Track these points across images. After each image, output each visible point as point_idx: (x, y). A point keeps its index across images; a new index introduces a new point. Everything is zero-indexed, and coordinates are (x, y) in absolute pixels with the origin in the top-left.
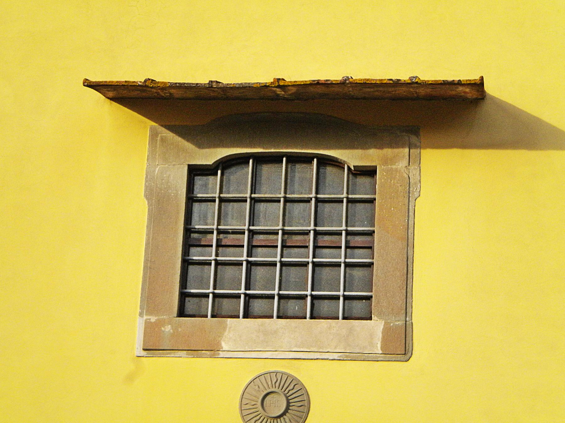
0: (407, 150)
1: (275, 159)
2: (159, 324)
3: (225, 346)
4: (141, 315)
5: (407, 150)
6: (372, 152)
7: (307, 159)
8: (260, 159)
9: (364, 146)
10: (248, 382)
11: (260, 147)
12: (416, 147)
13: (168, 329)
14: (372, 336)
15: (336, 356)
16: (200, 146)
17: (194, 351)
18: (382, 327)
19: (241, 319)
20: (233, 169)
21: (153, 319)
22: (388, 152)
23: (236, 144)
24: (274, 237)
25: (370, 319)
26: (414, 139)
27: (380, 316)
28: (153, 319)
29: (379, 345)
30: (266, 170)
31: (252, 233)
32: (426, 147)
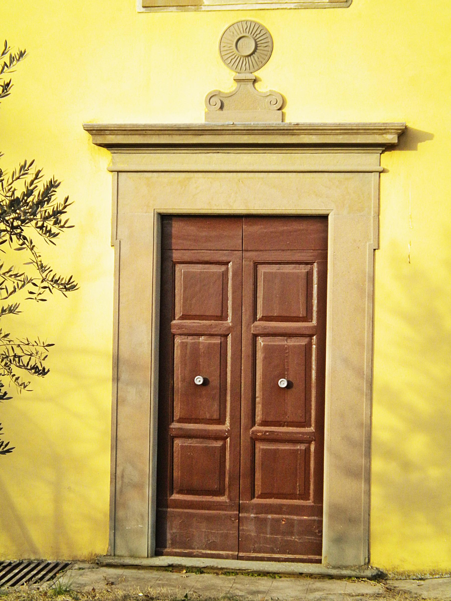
15: (292, 6)
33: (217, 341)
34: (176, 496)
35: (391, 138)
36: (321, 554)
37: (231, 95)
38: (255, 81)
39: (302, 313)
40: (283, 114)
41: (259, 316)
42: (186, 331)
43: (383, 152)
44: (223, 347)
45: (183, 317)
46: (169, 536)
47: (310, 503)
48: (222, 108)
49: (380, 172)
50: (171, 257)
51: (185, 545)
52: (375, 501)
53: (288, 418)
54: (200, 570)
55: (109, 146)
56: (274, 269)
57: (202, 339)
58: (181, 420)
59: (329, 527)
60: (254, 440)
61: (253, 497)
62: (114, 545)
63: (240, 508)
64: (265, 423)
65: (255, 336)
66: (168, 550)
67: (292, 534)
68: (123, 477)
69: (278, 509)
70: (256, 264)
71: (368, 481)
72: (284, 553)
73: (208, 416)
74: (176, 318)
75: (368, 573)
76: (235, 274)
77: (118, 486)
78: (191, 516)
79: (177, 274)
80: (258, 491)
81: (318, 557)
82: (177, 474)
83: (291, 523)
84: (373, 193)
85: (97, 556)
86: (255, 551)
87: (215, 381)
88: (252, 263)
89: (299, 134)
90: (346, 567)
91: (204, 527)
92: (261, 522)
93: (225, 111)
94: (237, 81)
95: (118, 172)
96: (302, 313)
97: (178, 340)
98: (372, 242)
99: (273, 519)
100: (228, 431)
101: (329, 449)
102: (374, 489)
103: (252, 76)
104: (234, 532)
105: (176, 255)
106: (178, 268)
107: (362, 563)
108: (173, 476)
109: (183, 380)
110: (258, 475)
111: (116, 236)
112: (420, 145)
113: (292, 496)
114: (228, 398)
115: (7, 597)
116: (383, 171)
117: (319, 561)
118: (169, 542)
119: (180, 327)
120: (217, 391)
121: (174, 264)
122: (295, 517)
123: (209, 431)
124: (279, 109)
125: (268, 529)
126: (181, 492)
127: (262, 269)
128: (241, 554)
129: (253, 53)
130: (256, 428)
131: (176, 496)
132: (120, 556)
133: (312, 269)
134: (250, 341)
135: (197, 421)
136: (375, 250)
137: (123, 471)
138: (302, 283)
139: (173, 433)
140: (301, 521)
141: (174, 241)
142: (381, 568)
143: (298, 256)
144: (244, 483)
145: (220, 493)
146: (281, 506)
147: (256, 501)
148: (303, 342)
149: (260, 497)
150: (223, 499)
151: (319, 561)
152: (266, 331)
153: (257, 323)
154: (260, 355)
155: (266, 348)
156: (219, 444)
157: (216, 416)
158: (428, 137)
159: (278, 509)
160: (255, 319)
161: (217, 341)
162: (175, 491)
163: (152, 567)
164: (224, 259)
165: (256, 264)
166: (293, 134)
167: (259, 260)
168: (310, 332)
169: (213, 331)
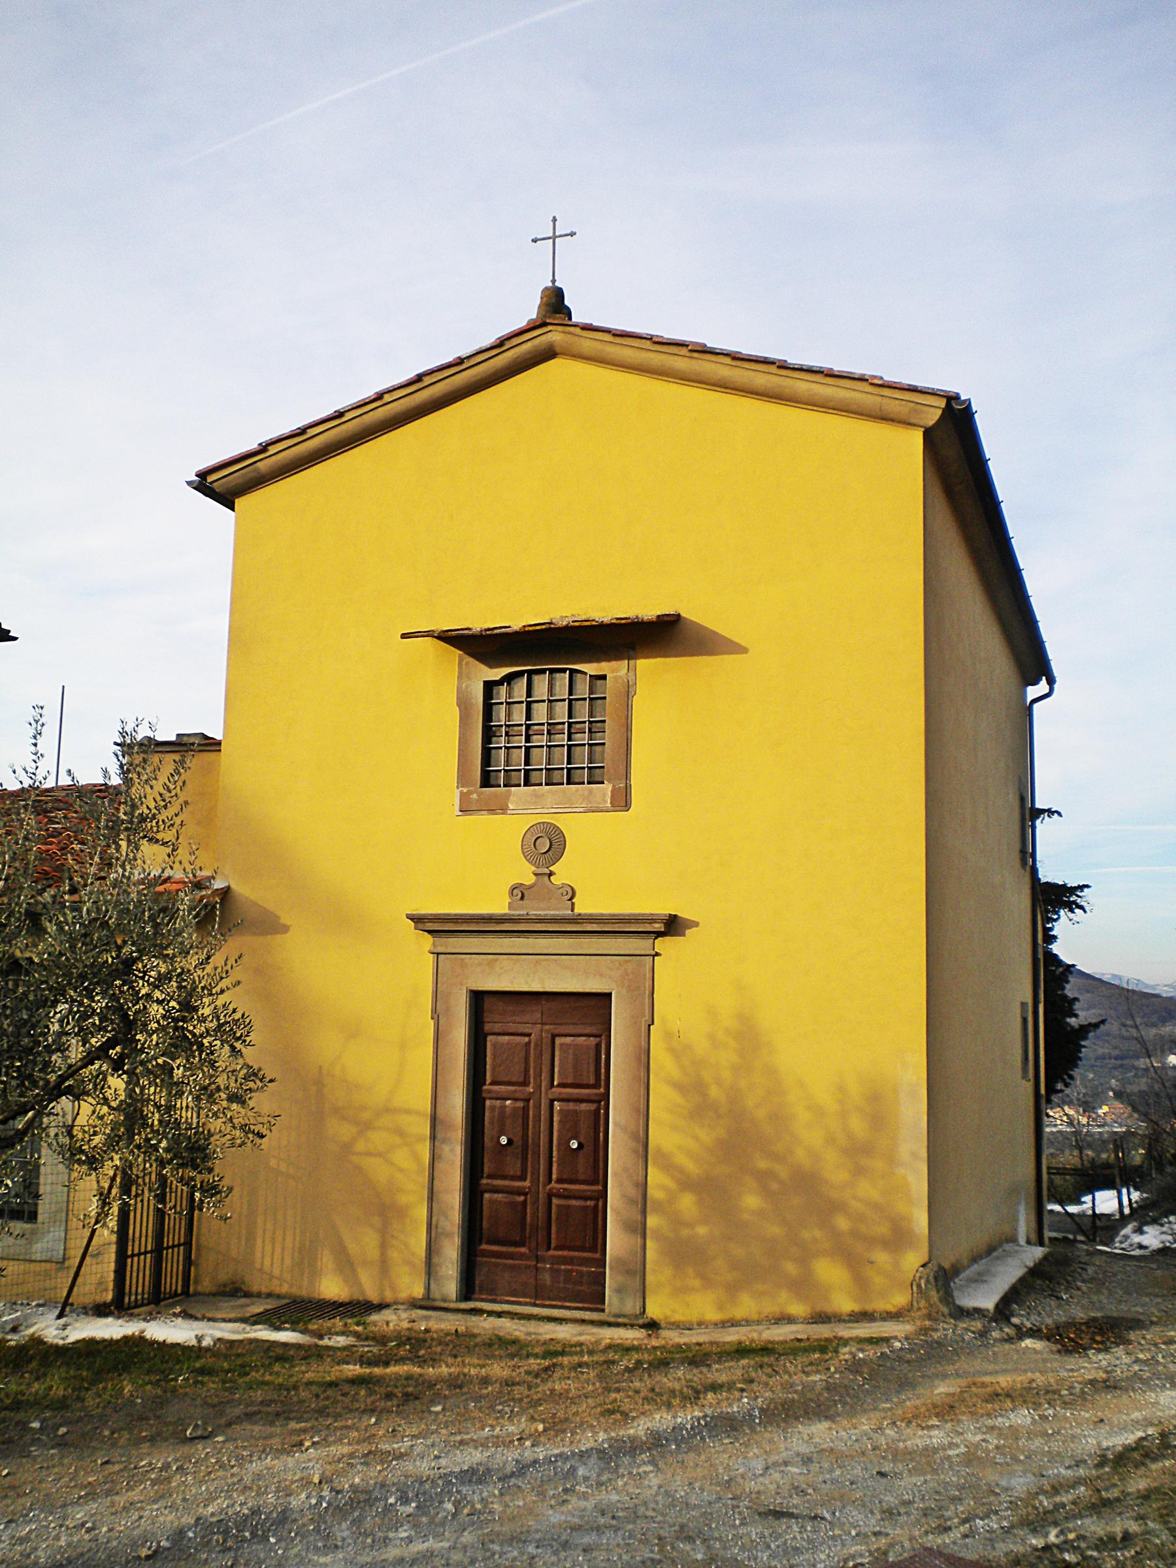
0: (626, 662)
1: (543, 671)
2: (469, 793)
3: (511, 807)
4: (458, 787)
5: (626, 662)
6: (604, 664)
7: (563, 671)
8: (531, 673)
9: (598, 661)
10: (639, 915)
11: (529, 665)
12: (633, 659)
13: (475, 796)
14: (604, 795)
15: (581, 810)
16: (491, 667)
17: (492, 811)
18: (610, 789)
19: (522, 788)
20: (516, 680)
21: (465, 790)
22: (614, 664)
23: (40, 942)
24: (583, 725)
25: (603, 783)
26: (631, 653)
27: (609, 782)
28: (465, 790)
29: (609, 801)
30: (536, 678)
31: (570, 724)
32: (639, 659)
33: (520, 1104)
34: (484, 1247)
35: (659, 927)
36: (604, 1303)
37: (531, 887)
38: (551, 874)
39: (592, 1081)
40: (573, 904)
41: (556, 1083)
42: (494, 1096)
43: (656, 938)
44: (525, 1110)
45: (493, 1083)
46: (477, 1282)
47: (598, 1256)
48: (522, 898)
49: (654, 956)
50: (483, 1029)
51: (492, 1291)
52: (650, 1254)
53: (581, 1177)
54: (499, 1315)
55: (429, 932)
56: (569, 1040)
57: (508, 1102)
58: (490, 1177)
59: (610, 1277)
60: (550, 1196)
61: (549, 1249)
62: (428, 1288)
63: (538, 1259)
64: (559, 1181)
65: (552, 1101)
66: (476, 1296)
67: (581, 1284)
68: (437, 1227)
69: (569, 1261)
70: (554, 1037)
71: (644, 1237)
72: (575, 1301)
73: (512, 1173)
74: (488, 1082)
75: (641, 1321)
76: (536, 1045)
77: (433, 1235)
78: (496, 1265)
79: (489, 1044)
80: (553, 1244)
81: (600, 1306)
82: (485, 1224)
83: (581, 1274)
84: (649, 975)
85: (414, 1299)
86: (550, 1299)
87: (517, 1140)
88: (550, 1036)
89: (583, 923)
90: (624, 1316)
91: (506, 1276)
92: (554, 1272)
93: (525, 902)
94: (536, 874)
95: (438, 954)
96: (592, 1081)
97: (488, 1103)
98: (647, 1017)
99: (565, 1270)
100: (529, 1188)
101: (612, 1208)
102: (650, 1244)
103: (547, 871)
104: (532, 1281)
105: (487, 1027)
106: (489, 1038)
107: (638, 1313)
108: (645, 1224)
109: (492, 1139)
110: (554, 1229)
111: (434, 1011)
112: (688, 932)
113: (582, 1249)
114: (529, 1156)
115: (106, 1274)
116: (657, 954)
117: (603, 1310)
118: (477, 1289)
119: (490, 1091)
120: (519, 1150)
121: (486, 1035)
122: (585, 1269)
123: (514, 1187)
124: (570, 900)
125: (562, 1278)
126: (489, 1242)
127: (558, 1041)
128: (538, 1302)
129: (548, 850)
130: (553, 1184)
131: (484, 1247)
132: (434, 1300)
133: (601, 1042)
134: (548, 1105)
135: (504, 1177)
136: (649, 1026)
137: (437, 1221)
138: (592, 1053)
139: (484, 1188)
140: (589, 1273)
141: (485, 1014)
142: (655, 1317)
143: (587, 1030)
144: (541, 1234)
145: (521, 1244)
146: (572, 1258)
147: (551, 1252)
148: (592, 1107)
149: (555, 1249)
150: (523, 1250)
151: (603, 1310)
152: (562, 1096)
153: (554, 1090)
154: (556, 1118)
155: (561, 1111)
156: (522, 1198)
157: (519, 1173)
158: (696, 924)
159: (569, 1261)
160: (552, 1085)
161: (520, 1104)
162: (484, 1240)
163: (458, 1311)
164: (527, 1031)
165: (554, 1037)
166: (578, 923)
167: (556, 1032)
168: (597, 1098)
169: (517, 1095)
